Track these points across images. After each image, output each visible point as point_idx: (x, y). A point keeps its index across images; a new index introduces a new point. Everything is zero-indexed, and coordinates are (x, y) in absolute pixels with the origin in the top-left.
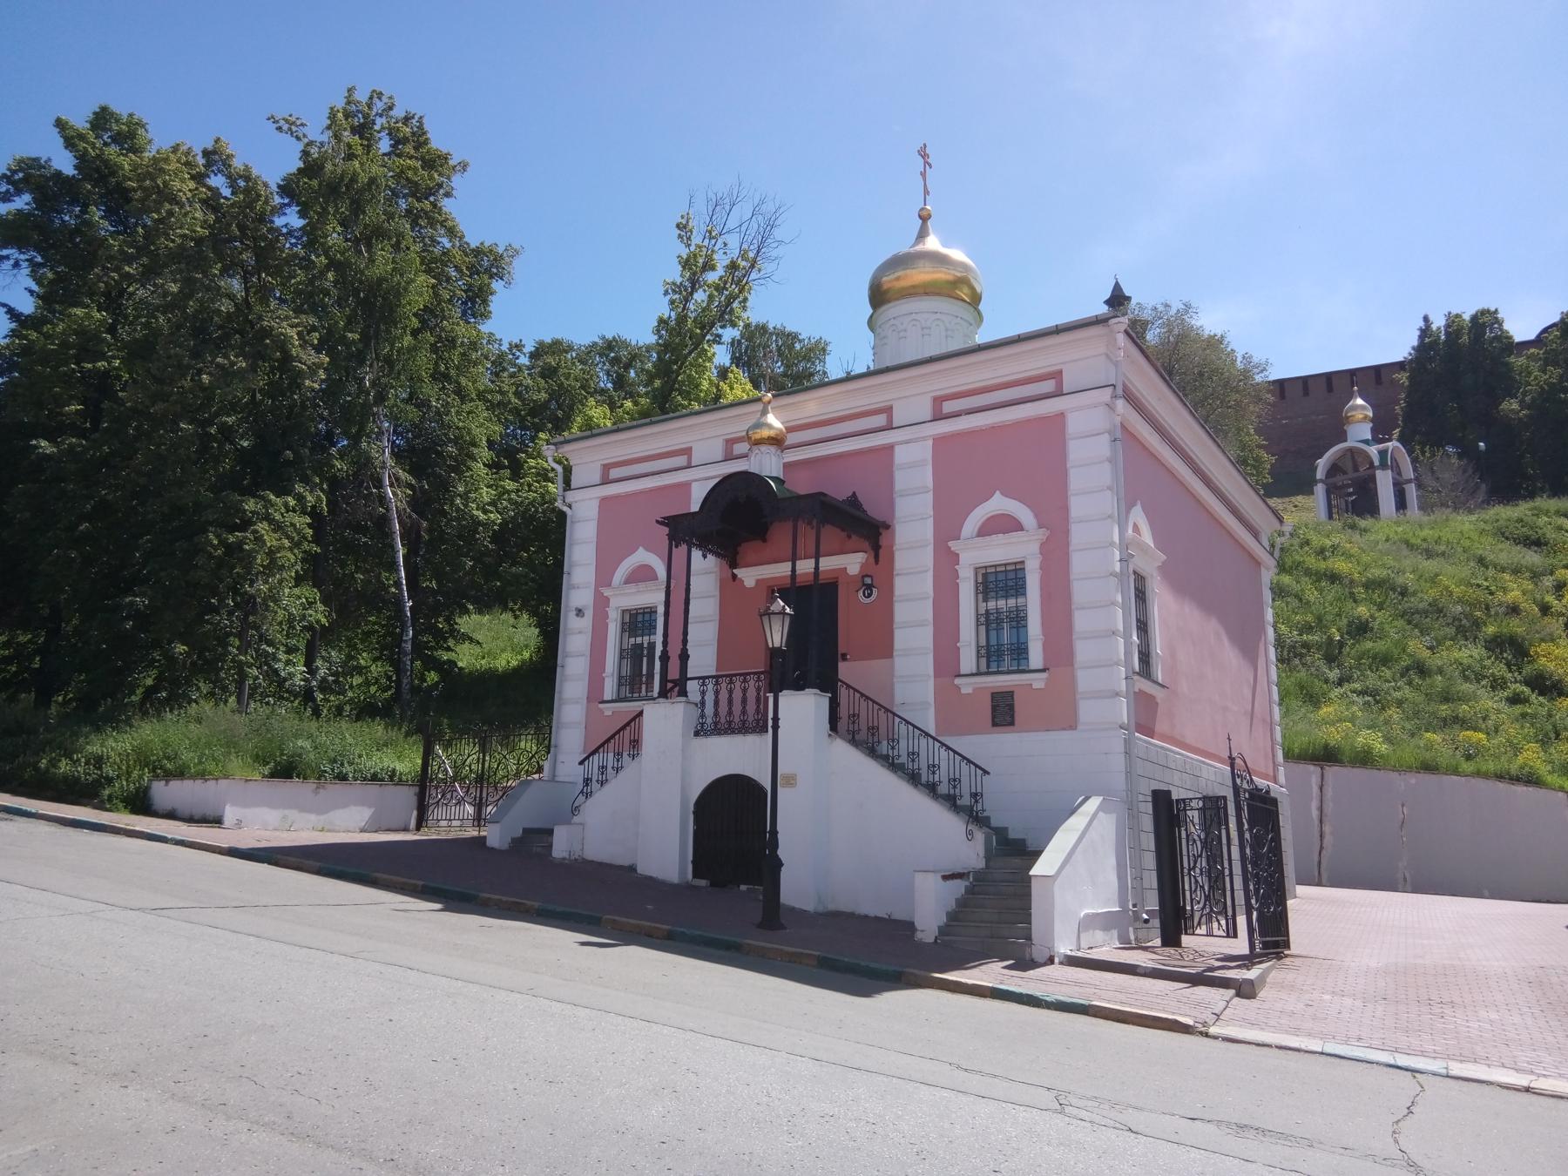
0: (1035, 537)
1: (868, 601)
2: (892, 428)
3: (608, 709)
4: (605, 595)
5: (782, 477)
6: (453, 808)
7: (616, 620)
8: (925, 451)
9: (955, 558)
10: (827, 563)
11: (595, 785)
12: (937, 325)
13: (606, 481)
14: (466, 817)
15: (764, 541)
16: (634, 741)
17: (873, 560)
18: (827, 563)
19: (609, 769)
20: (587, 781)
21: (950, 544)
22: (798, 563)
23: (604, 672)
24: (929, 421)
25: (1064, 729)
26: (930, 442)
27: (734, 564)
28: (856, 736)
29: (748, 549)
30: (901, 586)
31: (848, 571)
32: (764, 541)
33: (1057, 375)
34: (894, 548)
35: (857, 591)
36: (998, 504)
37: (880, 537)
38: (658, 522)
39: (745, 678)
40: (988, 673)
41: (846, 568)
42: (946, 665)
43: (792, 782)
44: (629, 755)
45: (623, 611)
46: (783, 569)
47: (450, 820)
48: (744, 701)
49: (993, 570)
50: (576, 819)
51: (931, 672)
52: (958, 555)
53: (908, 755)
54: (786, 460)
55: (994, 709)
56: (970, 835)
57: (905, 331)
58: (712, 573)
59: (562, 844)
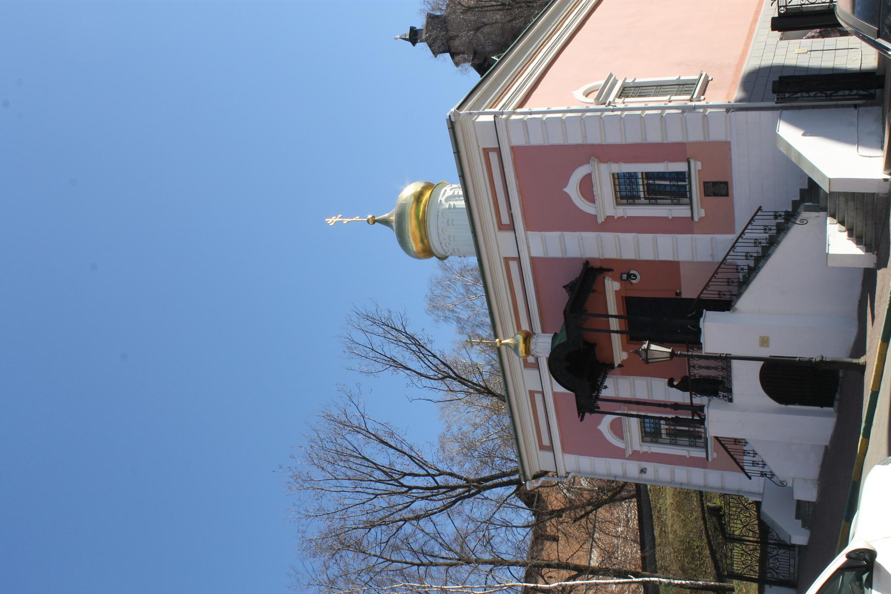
1: (638, 277)
3: (713, 455)
4: (631, 453)
5: (553, 335)
6: (781, 563)
7: (649, 447)
10: (612, 307)
11: (765, 470)
12: (446, 214)
13: (551, 448)
14: (788, 555)
16: (735, 442)
18: (612, 307)
20: (763, 474)
22: (612, 329)
23: (685, 456)
24: (515, 234)
26: (529, 233)
27: (611, 366)
28: (734, 293)
34: (602, 258)
35: (632, 284)
36: (572, 189)
37: (594, 267)
38: (582, 420)
39: (692, 367)
40: (691, 198)
41: (616, 291)
42: (685, 226)
44: (745, 446)
45: (618, 204)
46: (616, 339)
47: (790, 565)
48: (708, 368)
50: (790, 484)
51: (689, 236)
52: (607, 216)
53: (747, 259)
54: (541, 333)
55: (715, 195)
56: (804, 222)
57: (449, 237)
58: (617, 382)
59: (808, 493)
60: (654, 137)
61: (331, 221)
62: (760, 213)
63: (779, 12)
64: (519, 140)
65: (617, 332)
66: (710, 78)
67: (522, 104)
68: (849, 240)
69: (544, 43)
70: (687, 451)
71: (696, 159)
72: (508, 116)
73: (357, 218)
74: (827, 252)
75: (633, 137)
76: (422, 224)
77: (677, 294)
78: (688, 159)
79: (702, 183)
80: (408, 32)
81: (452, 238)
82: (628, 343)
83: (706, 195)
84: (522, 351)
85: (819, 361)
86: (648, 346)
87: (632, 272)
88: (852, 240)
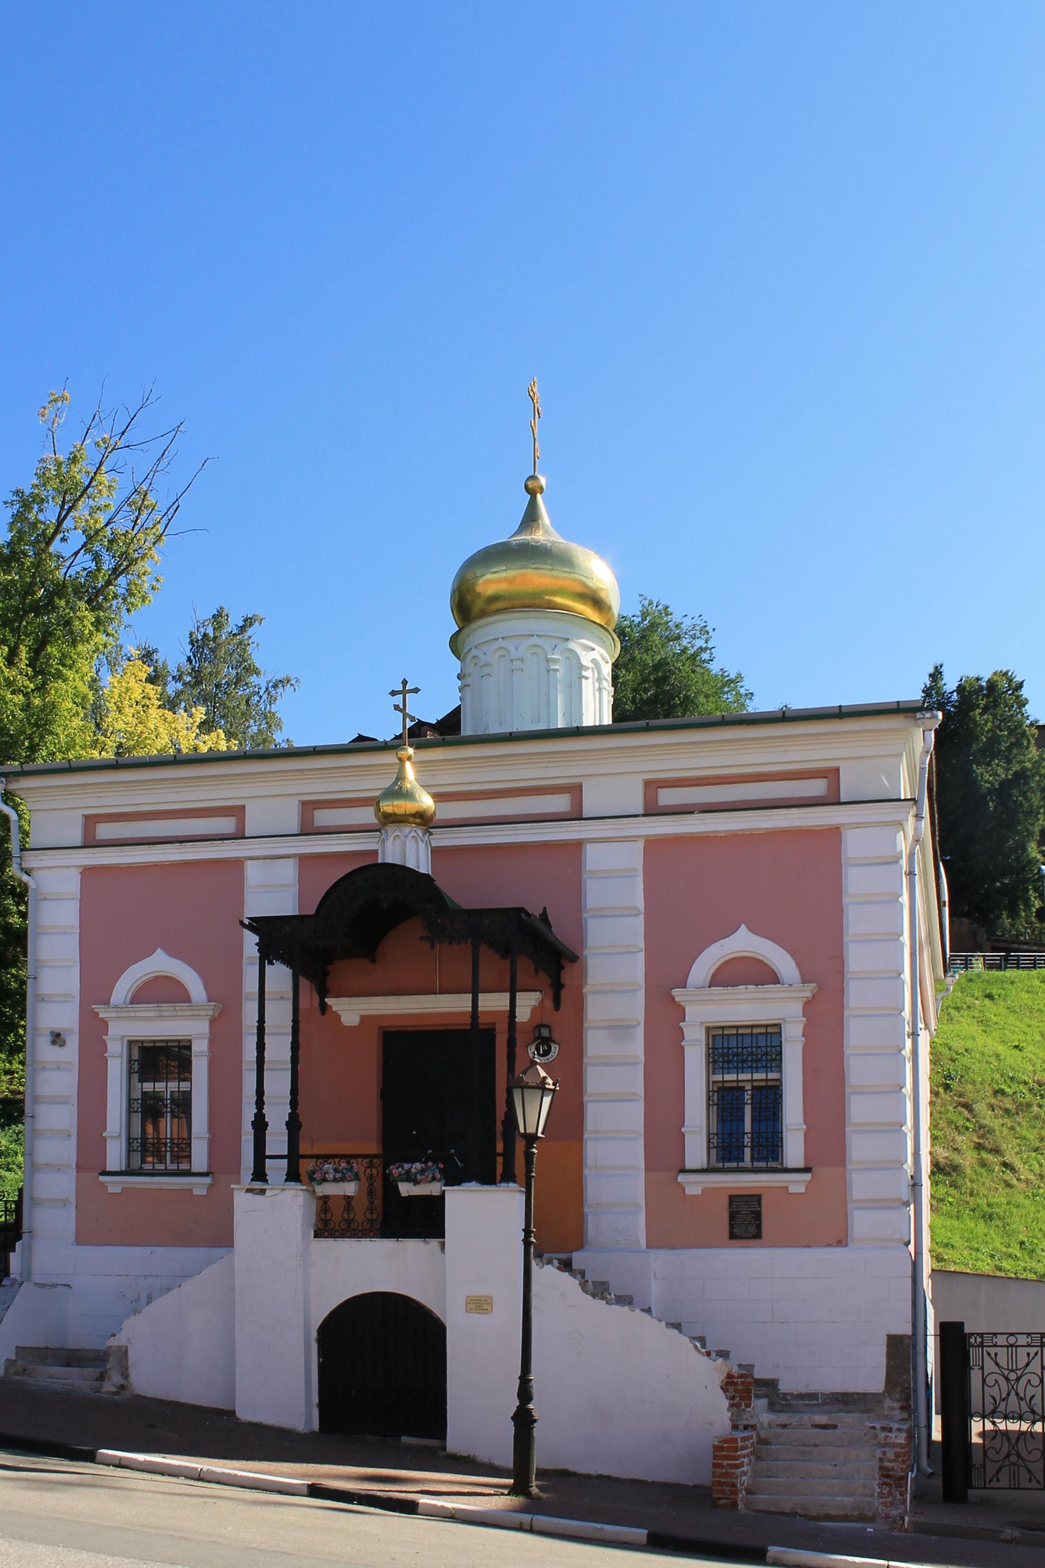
3: (115, 1185)
4: (101, 1016)
7: (121, 1056)
8: (633, 856)
9: (681, 1013)
15: (373, 960)
21: (675, 992)
22: (481, 996)
25: (830, 1245)
26: (641, 845)
29: (343, 970)
30: (596, 1044)
32: (373, 960)
33: (832, 775)
43: (485, 1307)
45: (131, 1043)
49: (735, 1032)
55: (733, 1216)
63: (973, 1334)
70: (120, 1134)
71: (210, 1187)
78: (212, 1173)
79: (758, 1193)
82: (380, 1027)
83: (732, 1199)
87: (555, 1049)
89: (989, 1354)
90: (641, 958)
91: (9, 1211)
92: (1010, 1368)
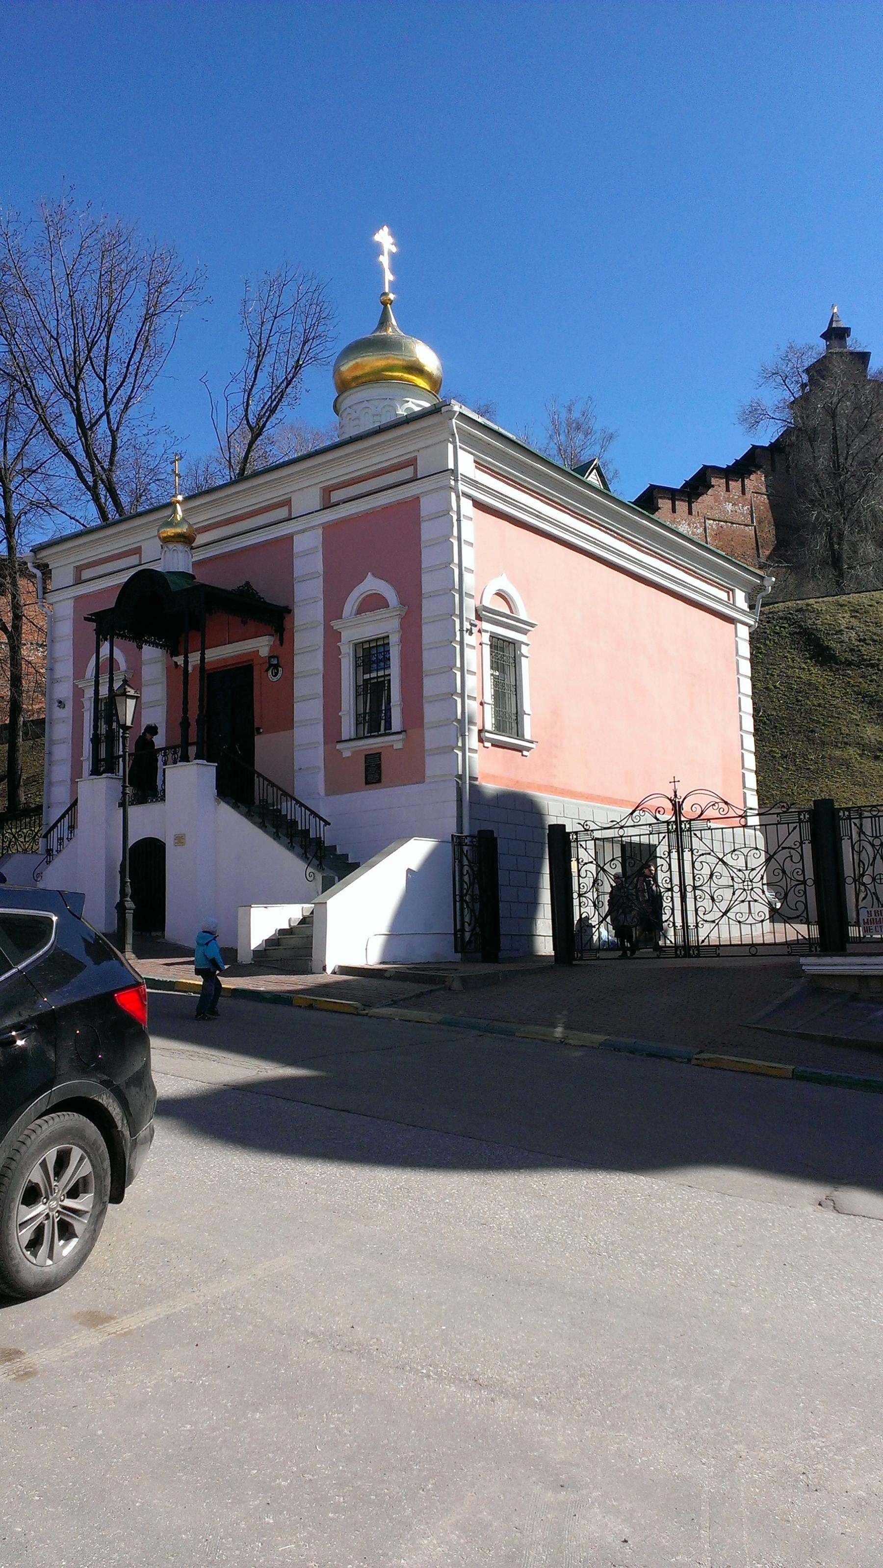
0: (395, 613)
1: (275, 679)
2: (292, 519)
5: (191, 572)
17: (278, 643)
19: (65, 839)
22: (206, 651)
26: (320, 531)
30: (300, 664)
31: (260, 654)
35: (267, 670)
38: (86, 619)
42: (332, 736)
45: (356, 645)
51: (321, 740)
57: (358, 419)
60: (430, 686)
61: (384, 238)
62: (322, 823)
64: (427, 507)
65: (203, 654)
66: (525, 753)
67: (479, 505)
68: (276, 931)
69: (611, 530)
72: (453, 487)
73: (389, 277)
74: (252, 906)
75: (430, 659)
76: (377, 378)
77: (258, 729)
80: (842, 324)
81: (356, 422)
84: (164, 532)
85: (125, 905)
86: (132, 697)
88: (275, 934)
89: (855, 824)
90: (321, 604)
91: (803, 822)
92: (874, 835)
